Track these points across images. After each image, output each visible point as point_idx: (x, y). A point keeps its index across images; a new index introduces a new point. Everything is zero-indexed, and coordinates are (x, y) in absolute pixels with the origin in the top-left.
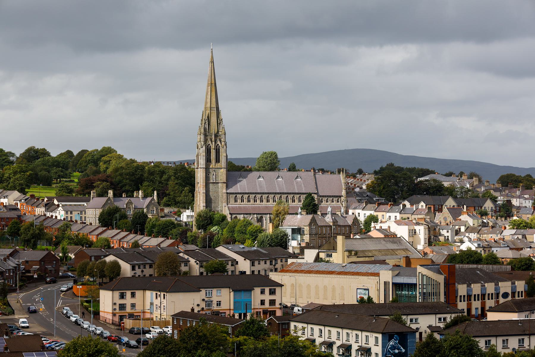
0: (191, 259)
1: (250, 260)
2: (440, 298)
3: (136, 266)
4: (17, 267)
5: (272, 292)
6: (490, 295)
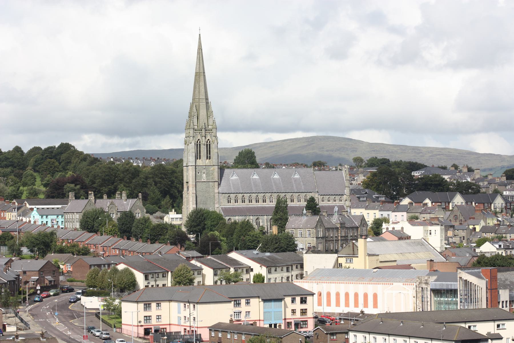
0: (204, 267)
1: (267, 267)
2: (482, 304)
3: (149, 275)
4: (17, 278)
5: (303, 301)
6: (505, 302)
